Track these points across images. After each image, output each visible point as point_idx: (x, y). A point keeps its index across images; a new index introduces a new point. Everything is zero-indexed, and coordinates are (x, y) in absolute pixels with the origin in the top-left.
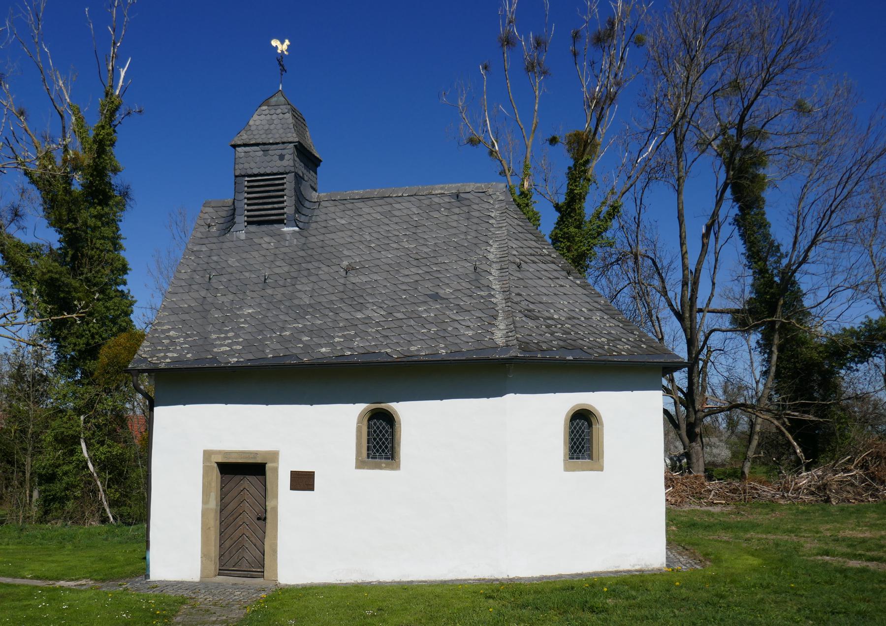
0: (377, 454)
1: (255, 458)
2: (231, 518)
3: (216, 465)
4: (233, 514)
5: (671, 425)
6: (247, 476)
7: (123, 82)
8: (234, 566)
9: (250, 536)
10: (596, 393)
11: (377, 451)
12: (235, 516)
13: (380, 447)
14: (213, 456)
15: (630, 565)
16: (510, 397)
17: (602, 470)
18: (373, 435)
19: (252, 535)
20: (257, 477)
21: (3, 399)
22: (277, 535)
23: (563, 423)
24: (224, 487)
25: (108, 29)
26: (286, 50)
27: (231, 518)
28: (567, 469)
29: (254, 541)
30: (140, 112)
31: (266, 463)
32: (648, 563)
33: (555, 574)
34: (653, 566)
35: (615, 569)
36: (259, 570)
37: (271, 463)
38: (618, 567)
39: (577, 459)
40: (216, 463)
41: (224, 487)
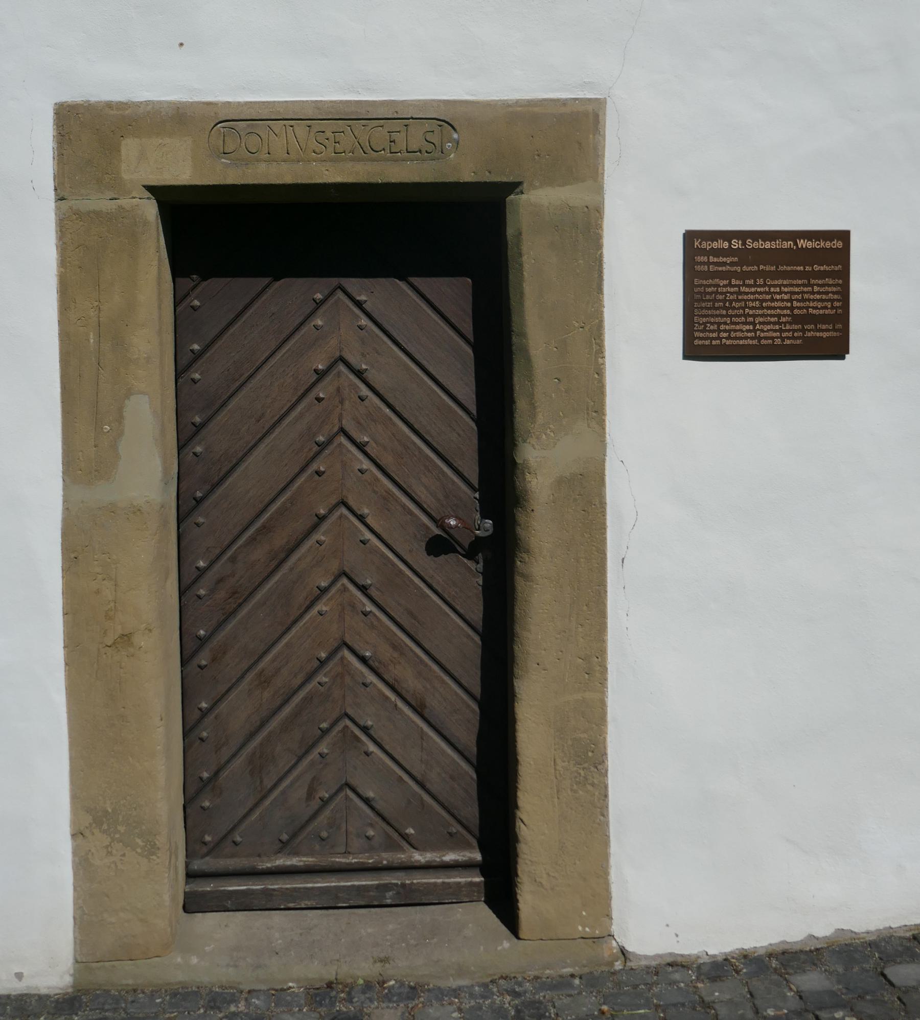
1: (433, 151)
2: (259, 554)
3: (150, 210)
4: (266, 529)
5: (380, 182)
6: (352, 284)
8: (284, 847)
9: (386, 652)
12: (280, 539)
14: (129, 147)
19: (396, 646)
20: (415, 280)
21: (692, 974)
22: (601, 653)
24: (198, 356)
27: (259, 554)
29: (411, 683)
31: (513, 187)
36: (450, 857)
37: (550, 181)
40: (153, 190)
41: (198, 356)
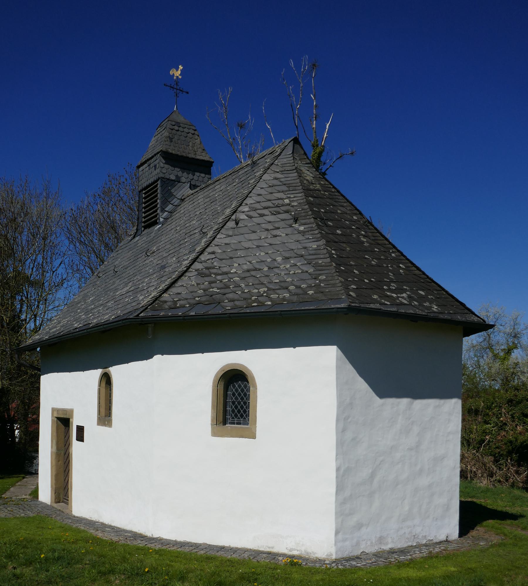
0: (242, 420)
7: (327, 134)
10: (249, 351)
11: (236, 416)
13: (239, 411)
15: (287, 548)
16: (157, 358)
17: (254, 437)
18: (232, 399)
23: (211, 384)
25: (311, 96)
26: (180, 75)
28: (215, 434)
30: (352, 153)
32: (309, 551)
33: (220, 545)
34: (317, 555)
35: (268, 550)
38: (273, 548)
39: (238, 424)
